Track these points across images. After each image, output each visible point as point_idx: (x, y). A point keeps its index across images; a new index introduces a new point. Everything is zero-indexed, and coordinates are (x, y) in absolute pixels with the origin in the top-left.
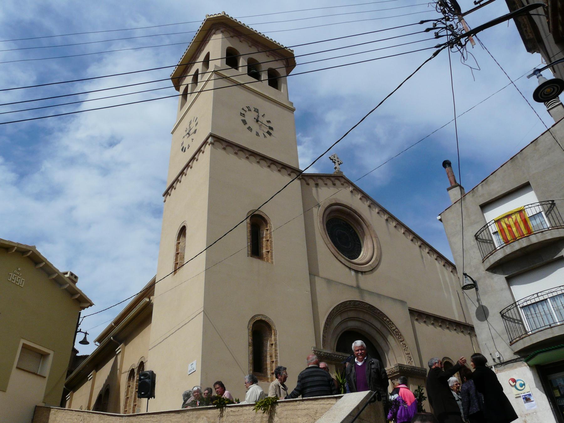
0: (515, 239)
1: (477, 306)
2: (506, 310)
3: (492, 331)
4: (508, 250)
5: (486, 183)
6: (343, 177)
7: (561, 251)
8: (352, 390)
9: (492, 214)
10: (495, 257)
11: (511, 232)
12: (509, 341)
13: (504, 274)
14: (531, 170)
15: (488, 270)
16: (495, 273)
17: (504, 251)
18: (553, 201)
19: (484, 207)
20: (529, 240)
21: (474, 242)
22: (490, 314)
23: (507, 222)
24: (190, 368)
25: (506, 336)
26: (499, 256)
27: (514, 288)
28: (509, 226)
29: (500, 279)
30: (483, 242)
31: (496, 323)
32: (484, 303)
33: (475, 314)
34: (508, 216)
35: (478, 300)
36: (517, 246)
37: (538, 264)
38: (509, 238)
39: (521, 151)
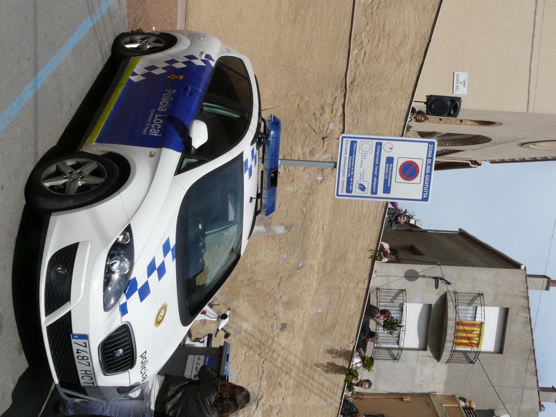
0: (457, 331)
1: (420, 274)
2: (405, 298)
3: (394, 278)
4: (451, 324)
5: (527, 322)
6: (123, 35)
7: (431, 351)
8: (155, 75)
9: (490, 317)
10: (452, 308)
11: (465, 331)
12: (380, 288)
13: (436, 305)
14: (511, 361)
15: (446, 293)
16: (440, 298)
17: (452, 320)
18: (474, 363)
19: (505, 313)
20: (450, 342)
21: (477, 291)
22: (408, 282)
23: (475, 332)
25: (385, 287)
26: (451, 314)
27: (422, 305)
28: (471, 332)
29: (433, 298)
30: (473, 299)
31: (400, 283)
32: (420, 279)
33: (413, 269)
34: (480, 335)
35: (424, 276)
36: (450, 331)
37: (430, 332)
38: (461, 328)
39: (535, 361)
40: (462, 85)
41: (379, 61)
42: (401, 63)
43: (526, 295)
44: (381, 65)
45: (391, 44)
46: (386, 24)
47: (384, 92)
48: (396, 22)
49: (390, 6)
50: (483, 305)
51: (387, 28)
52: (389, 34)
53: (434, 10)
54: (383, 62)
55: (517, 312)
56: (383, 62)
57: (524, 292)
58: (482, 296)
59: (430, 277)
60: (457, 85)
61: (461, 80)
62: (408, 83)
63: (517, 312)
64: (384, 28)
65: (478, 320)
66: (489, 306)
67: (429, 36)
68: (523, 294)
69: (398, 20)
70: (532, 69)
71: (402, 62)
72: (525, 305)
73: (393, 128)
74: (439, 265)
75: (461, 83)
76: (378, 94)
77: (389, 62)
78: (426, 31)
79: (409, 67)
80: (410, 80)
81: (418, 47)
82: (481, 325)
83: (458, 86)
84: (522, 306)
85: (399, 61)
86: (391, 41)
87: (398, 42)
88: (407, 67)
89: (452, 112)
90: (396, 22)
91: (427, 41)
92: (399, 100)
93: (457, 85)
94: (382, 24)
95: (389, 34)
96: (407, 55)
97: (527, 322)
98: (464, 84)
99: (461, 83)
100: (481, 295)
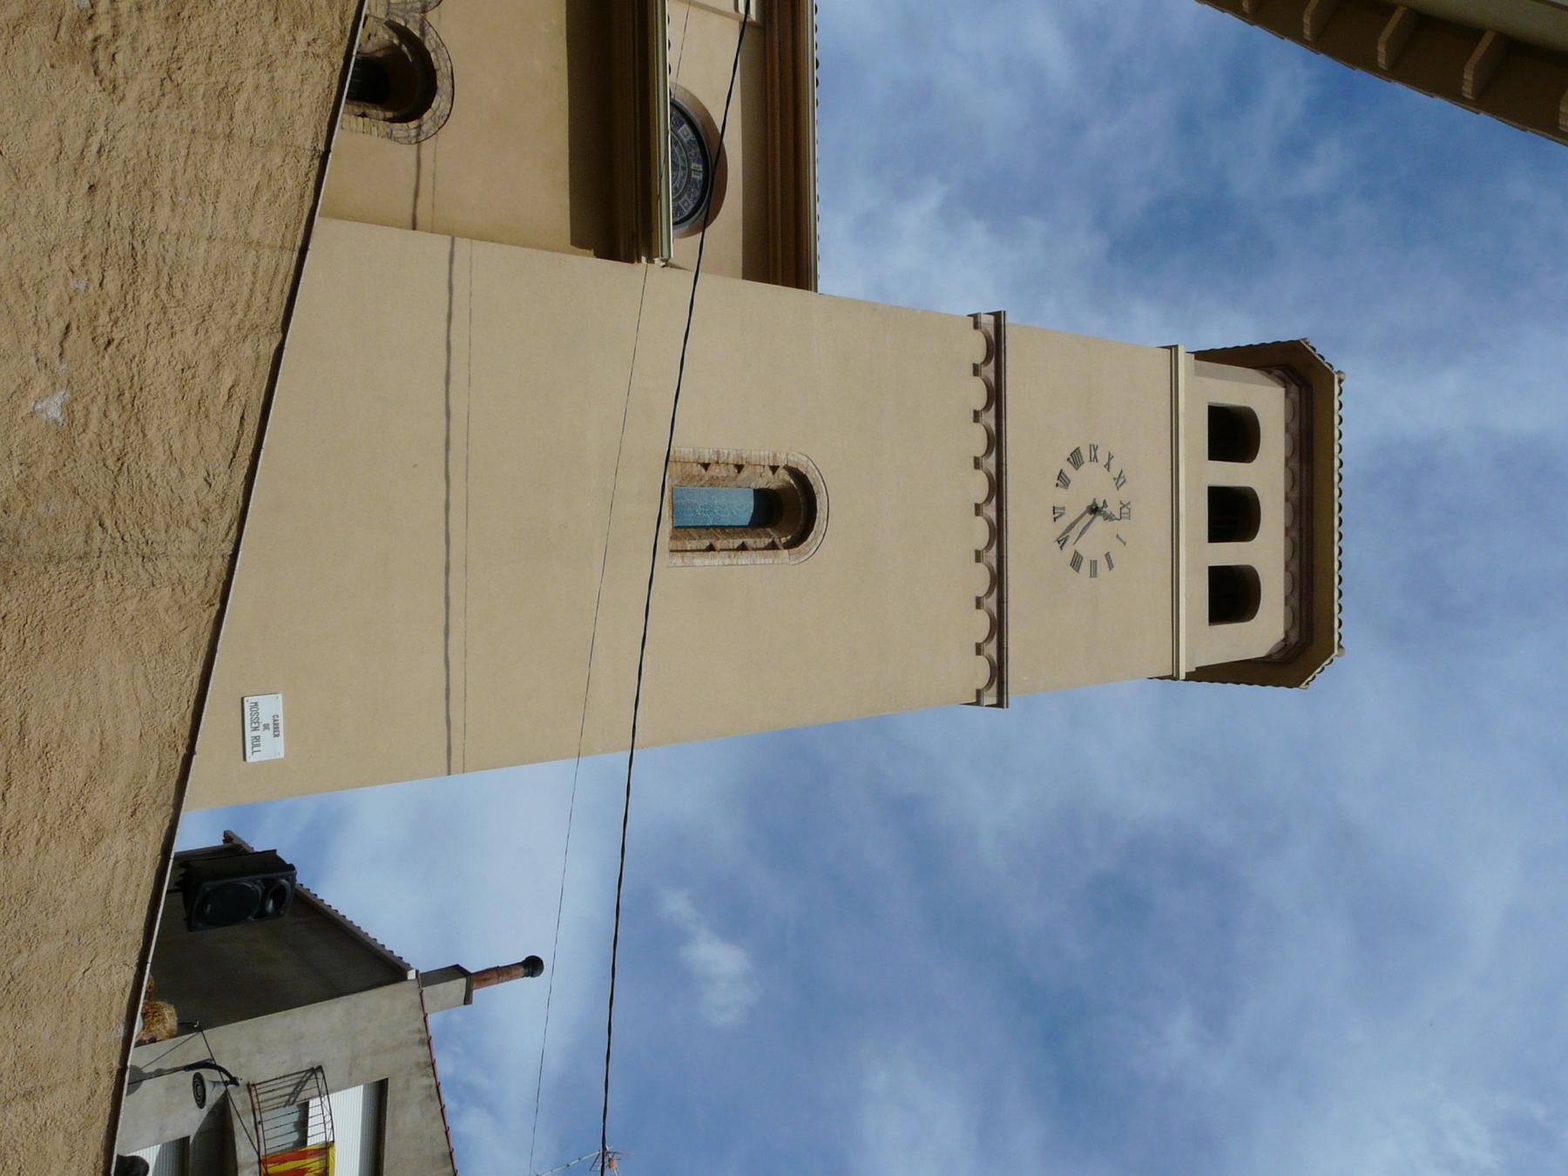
13: (200, 1133)
19: (379, 1094)
24: (270, 706)
29: (189, 1121)
35: (159, 1073)
40: (271, 732)
41: (14, 851)
42: (96, 841)
43: (424, 1035)
44: (24, 863)
45: (54, 785)
46: (31, 719)
47: (45, 948)
48: (67, 706)
49: (38, 658)
50: (324, 1092)
51: (34, 735)
52: (43, 753)
53: (193, 658)
54: (29, 850)
55: (408, 1081)
56: (29, 850)
57: (419, 1031)
58: (320, 1075)
59: (175, 1070)
60: (255, 733)
61: (266, 718)
62: (129, 898)
63: (408, 1081)
64: (22, 735)
65: (315, 1139)
66: (339, 1089)
67: (186, 734)
68: (417, 1037)
69: (75, 700)
70: (451, 659)
71: (99, 834)
72: (423, 1060)
73: (87, 1056)
74: (200, 1029)
75: (266, 727)
76: (20, 962)
77: (52, 845)
78: (174, 720)
79: (128, 845)
80: (133, 887)
81: (152, 776)
82: (326, 1149)
83: (257, 738)
84: (418, 1064)
85: (88, 834)
86: (55, 775)
87: (81, 774)
88: (119, 847)
89: (270, 905)
90: (67, 706)
91: (182, 751)
92: (99, 961)
93: (255, 733)
94: (13, 724)
95: (43, 753)
96: (116, 810)
97: (430, 1096)
98: (276, 728)
99: (266, 727)
100: (316, 1070)
